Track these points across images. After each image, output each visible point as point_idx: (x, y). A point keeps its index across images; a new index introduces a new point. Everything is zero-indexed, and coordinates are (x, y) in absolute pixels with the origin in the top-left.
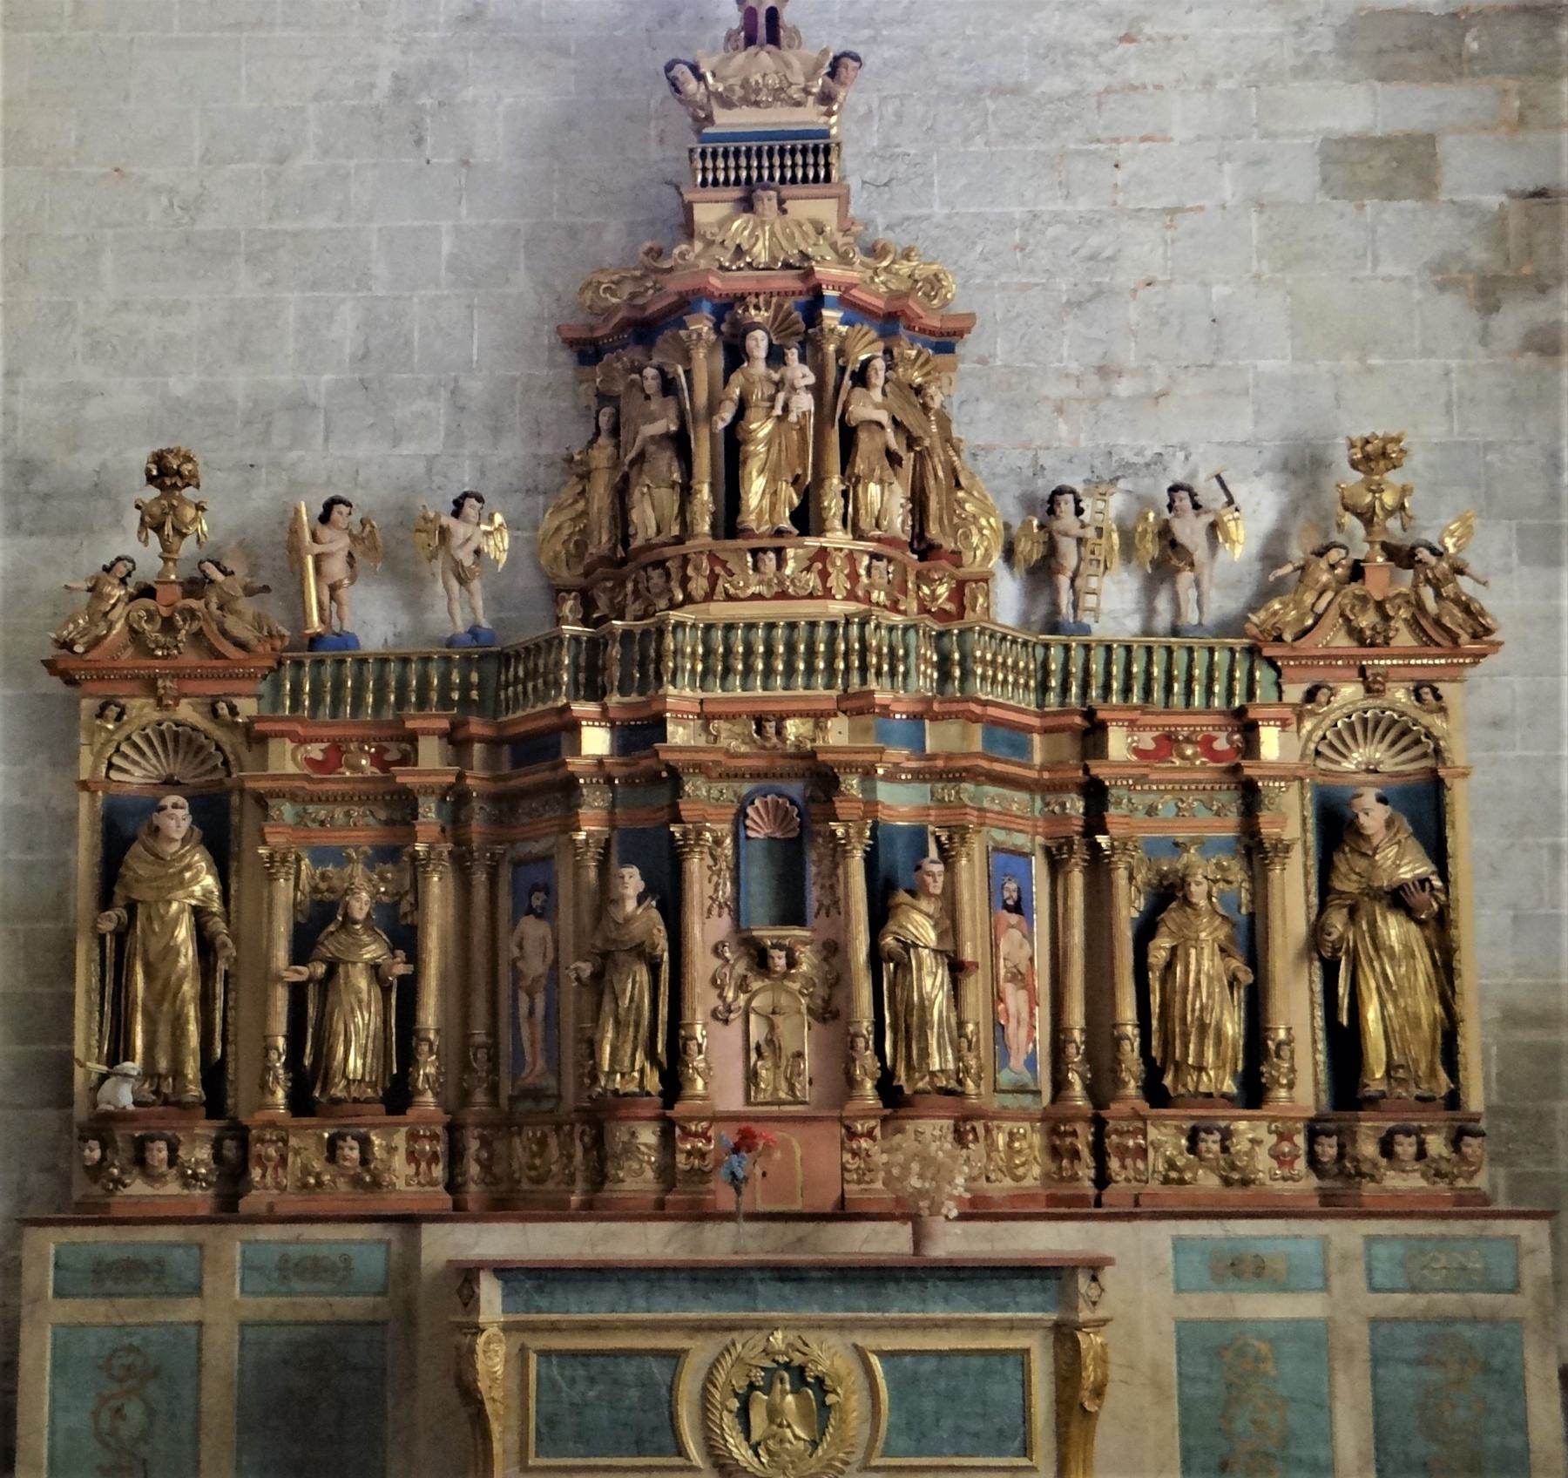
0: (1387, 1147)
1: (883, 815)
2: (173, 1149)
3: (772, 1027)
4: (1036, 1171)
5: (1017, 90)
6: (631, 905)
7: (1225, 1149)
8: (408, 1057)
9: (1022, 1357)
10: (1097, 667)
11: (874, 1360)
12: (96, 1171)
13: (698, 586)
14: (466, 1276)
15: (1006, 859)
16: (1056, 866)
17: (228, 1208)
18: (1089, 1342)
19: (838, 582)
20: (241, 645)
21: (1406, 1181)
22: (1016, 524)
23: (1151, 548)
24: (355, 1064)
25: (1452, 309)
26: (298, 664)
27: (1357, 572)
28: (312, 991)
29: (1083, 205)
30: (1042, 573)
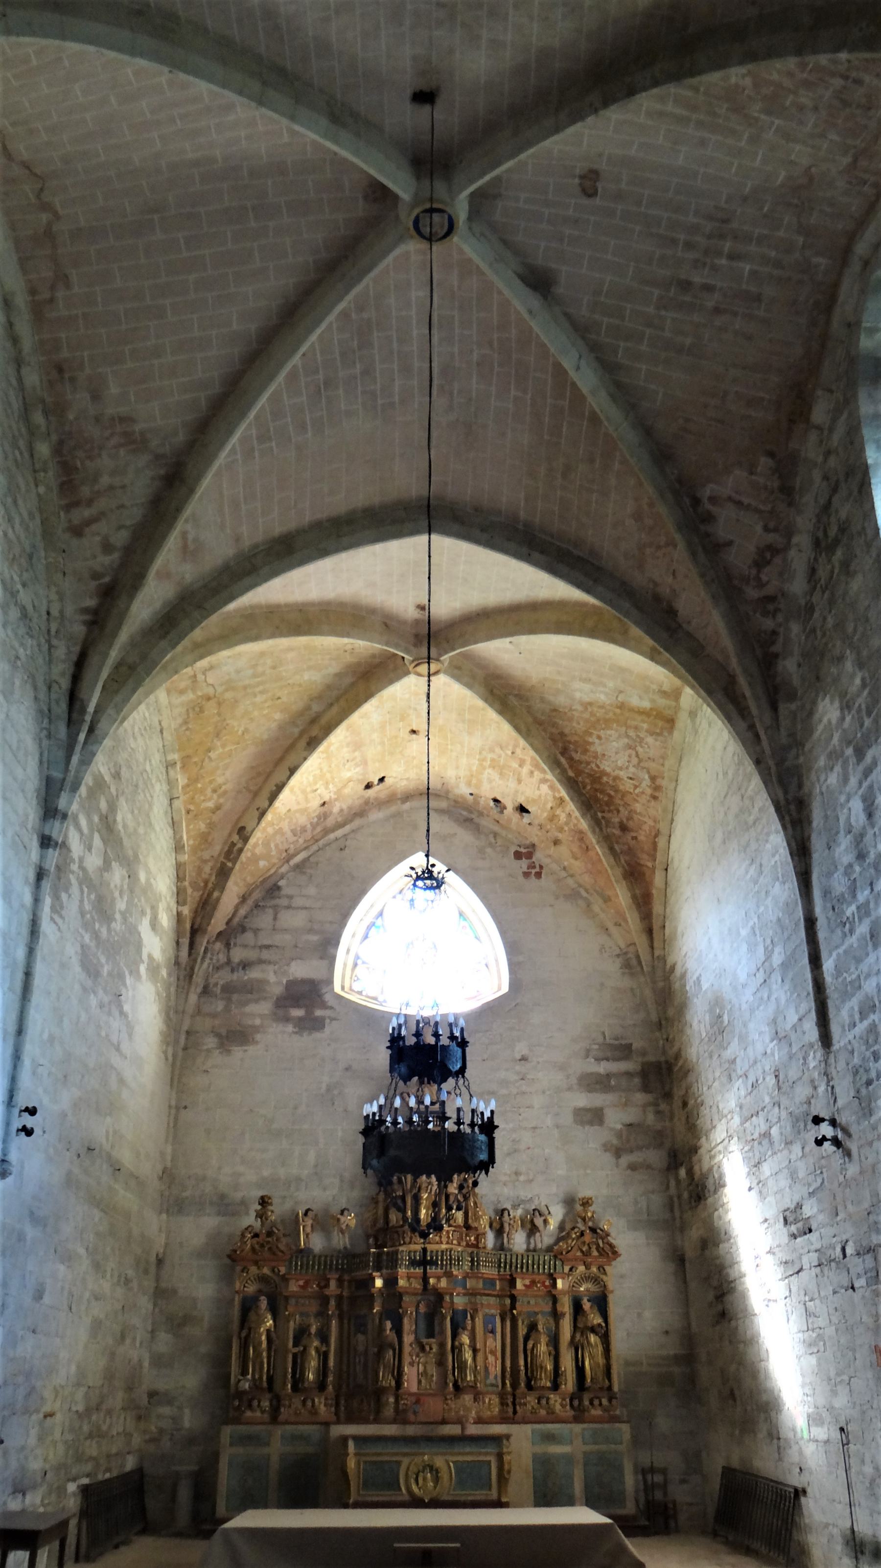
0: (591, 1403)
1: (455, 1306)
2: (259, 1402)
3: (425, 1367)
4: (497, 1410)
6: (388, 1332)
7: (547, 1403)
9: (489, 1462)
10: (514, 1260)
11: (451, 1464)
12: (238, 1408)
13: (407, 1240)
14: (344, 1439)
15: (489, 1320)
16: (503, 1320)
18: (506, 1458)
19: (444, 1239)
20: (282, 1252)
21: (596, 1412)
22: (493, 1218)
23: (529, 1226)
24: (311, 1377)
25: (608, 1158)
26: (297, 1257)
27: (582, 1234)
28: (299, 1356)
29: (511, 1125)
30: (499, 1232)
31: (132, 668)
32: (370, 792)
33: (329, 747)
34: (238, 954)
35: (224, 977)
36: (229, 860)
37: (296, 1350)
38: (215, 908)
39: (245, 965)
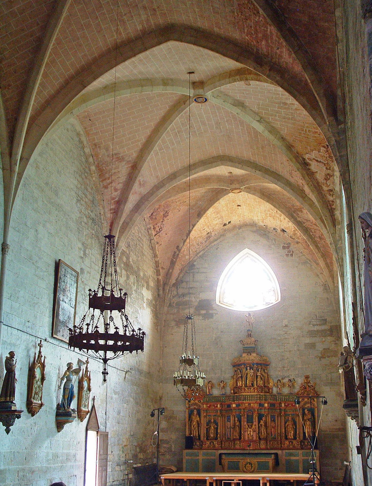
5: (275, 339)
8: (217, 435)
13: (243, 391)
17: (201, 449)
31: (128, 224)
32: (225, 227)
33: (207, 215)
34: (181, 291)
35: (175, 300)
36: (174, 258)
37: (207, 427)
38: (171, 276)
39: (184, 295)
